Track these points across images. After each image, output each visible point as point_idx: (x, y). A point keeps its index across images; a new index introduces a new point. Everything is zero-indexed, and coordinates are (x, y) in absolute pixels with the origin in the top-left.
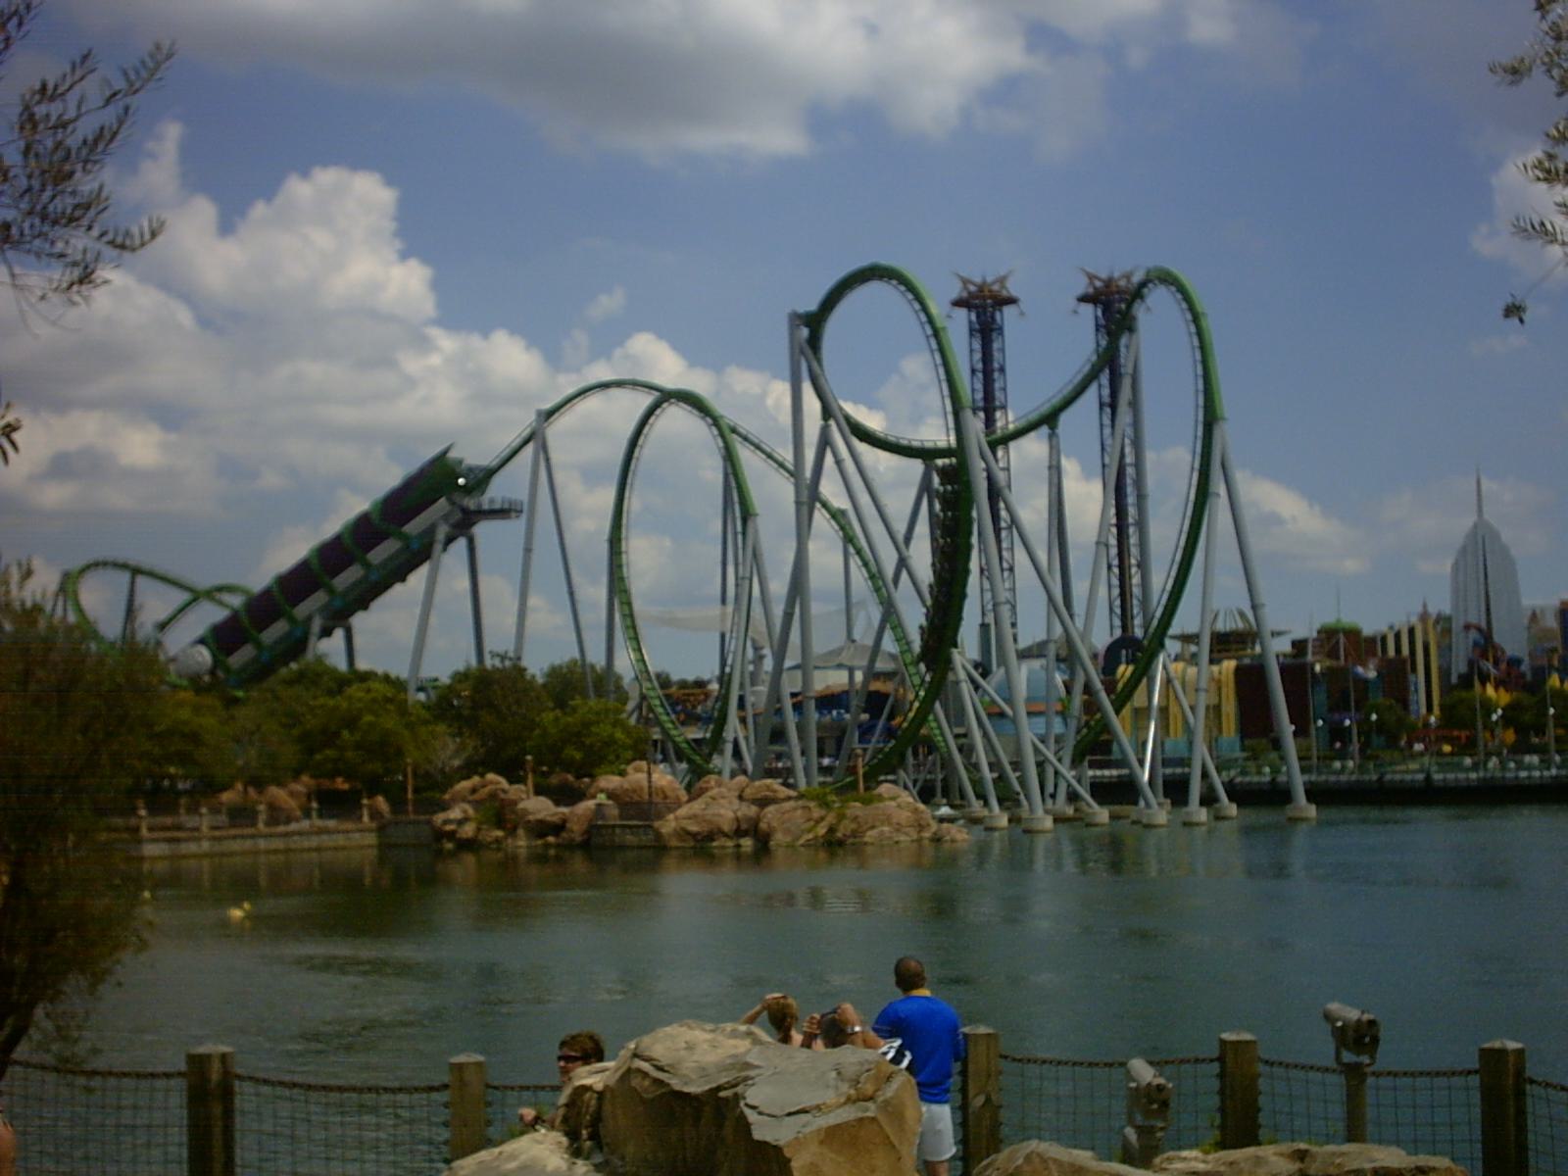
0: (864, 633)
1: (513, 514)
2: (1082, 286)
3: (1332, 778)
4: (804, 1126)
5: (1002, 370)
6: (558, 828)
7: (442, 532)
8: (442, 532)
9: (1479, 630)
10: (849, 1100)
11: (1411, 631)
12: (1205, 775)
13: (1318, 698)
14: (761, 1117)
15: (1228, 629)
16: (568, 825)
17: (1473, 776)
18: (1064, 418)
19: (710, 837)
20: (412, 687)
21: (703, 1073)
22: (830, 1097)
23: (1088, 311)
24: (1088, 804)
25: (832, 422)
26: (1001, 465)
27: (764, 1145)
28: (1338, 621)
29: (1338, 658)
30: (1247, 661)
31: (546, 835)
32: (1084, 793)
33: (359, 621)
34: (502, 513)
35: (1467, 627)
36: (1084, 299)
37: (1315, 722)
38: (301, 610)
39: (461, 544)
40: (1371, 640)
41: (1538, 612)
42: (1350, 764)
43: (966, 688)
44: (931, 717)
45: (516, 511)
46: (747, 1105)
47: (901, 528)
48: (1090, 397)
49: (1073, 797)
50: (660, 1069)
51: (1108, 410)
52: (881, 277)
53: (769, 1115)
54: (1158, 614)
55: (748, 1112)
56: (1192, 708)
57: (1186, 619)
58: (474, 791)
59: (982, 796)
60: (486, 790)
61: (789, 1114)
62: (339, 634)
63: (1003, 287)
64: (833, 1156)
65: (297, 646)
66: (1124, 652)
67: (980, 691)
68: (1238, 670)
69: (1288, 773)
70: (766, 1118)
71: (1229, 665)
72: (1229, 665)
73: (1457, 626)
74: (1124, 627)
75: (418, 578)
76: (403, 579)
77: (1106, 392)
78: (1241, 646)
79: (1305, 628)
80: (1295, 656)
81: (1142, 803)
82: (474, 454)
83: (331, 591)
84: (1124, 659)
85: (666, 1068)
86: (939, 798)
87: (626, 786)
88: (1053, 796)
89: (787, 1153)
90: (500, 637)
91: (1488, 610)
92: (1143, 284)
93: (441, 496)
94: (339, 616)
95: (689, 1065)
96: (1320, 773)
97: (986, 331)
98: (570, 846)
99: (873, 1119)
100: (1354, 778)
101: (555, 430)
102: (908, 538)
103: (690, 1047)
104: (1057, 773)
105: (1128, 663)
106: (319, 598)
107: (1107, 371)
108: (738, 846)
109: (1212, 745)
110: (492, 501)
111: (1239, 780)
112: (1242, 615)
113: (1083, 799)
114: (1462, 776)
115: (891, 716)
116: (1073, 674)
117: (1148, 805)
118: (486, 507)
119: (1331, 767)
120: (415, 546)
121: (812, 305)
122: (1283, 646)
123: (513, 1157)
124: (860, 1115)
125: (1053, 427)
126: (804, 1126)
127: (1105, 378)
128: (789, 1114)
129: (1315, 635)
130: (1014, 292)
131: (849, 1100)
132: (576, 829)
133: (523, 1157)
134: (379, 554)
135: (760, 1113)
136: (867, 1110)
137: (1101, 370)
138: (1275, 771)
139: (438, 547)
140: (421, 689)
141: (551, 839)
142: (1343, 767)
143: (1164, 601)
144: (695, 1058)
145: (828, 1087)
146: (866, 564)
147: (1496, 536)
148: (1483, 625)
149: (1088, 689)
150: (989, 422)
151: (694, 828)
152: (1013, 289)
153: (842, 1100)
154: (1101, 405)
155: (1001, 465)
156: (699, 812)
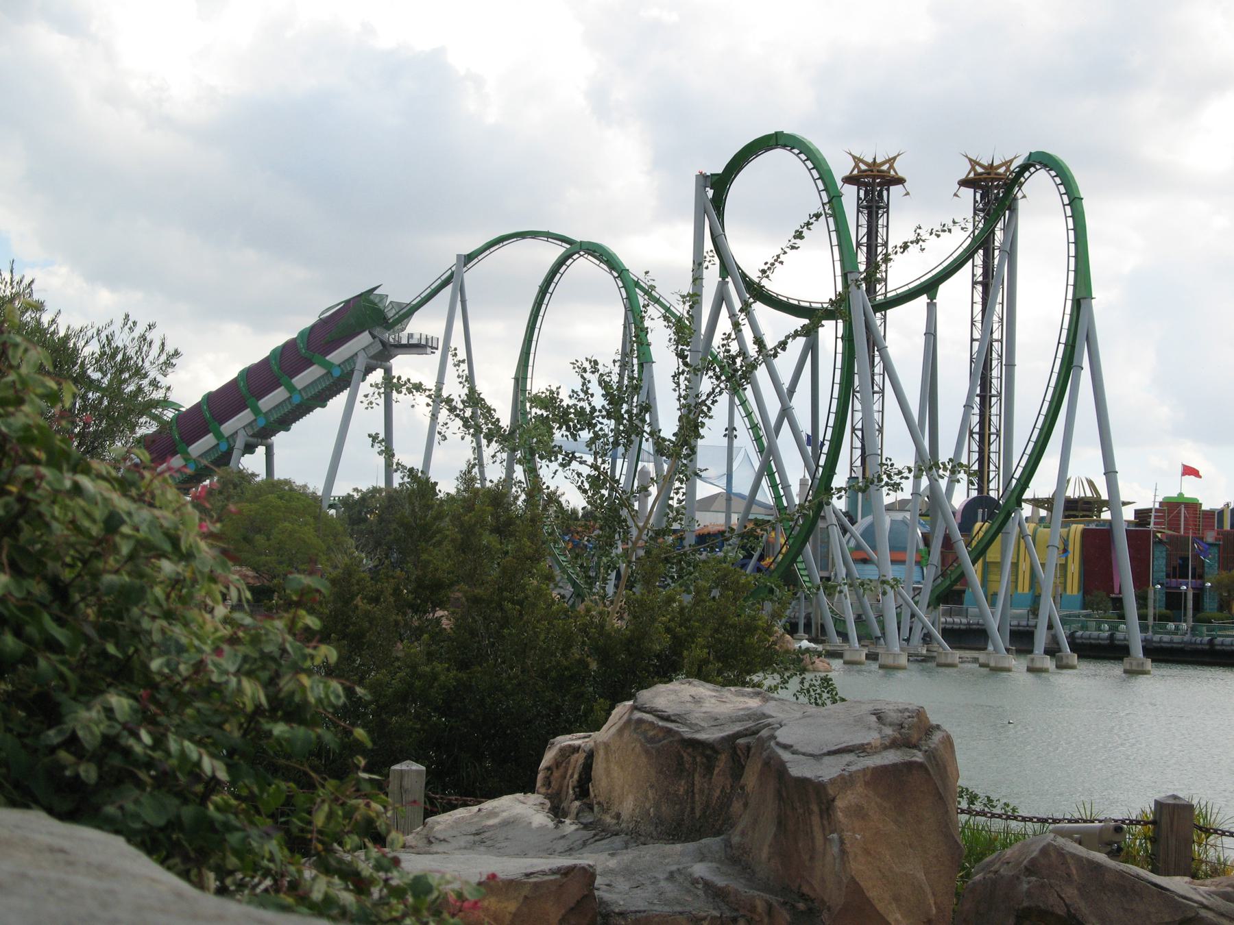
0: (742, 485)
1: (429, 350)
2: (964, 170)
3: (1166, 638)
4: (848, 765)
8: (360, 364)
10: (894, 744)
12: (1050, 627)
13: (1158, 563)
14: (795, 756)
15: (1076, 497)
18: (943, 289)
20: (325, 505)
21: (716, 721)
22: (872, 737)
23: (968, 193)
24: (940, 645)
25: (729, 279)
27: (803, 782)
28: (1181, 494)
29: (1177, 529)
30: (1093, 526)
32: (937, 634)
33: (279, 439)
36: (965, 183)
37: (1153, 586)
38: (228, 428)
40: (1210, 513)
42: (1184, 626)
43: (835, 532)
44: (800, 558)
45: (432, 348)
46: (778, 744)
47: (786, 381)
48: (963, 277)
49: (927, 638)
50: (667, 719)
51: (979, 288)
52: (784, 146)
53: (804, 754)
54: (1017, 475)
55: (780, 752)
56: (1043, 565)
57: (1042, 485)
59: (844, 636)
61: (830, 753)
62: (261, 450)
63: (891, 167)
64: (878, 800)
65: (224, 458)
66: (980, 511)
67: (848, 535)
68: (1085, 533)
69: (1128, 631)
70: (801, 757)
71: (1077, 528)
72: (1077, 528)
74: (980, 490)
75: (338, 402)
76: (323, 404)
77: (979, 271)
78: (1088, 513)
79: (1147, 501)
80: (1137, 525)
81: (991, 648)
82: (397, 292)
83: (256, 411)
84: (980, 517)
85: (673, 718)
86: (801, 633)
88: (908, 640)
89: (831, 791)
90: (409, 455)
92: (1024, 168)
93: (364, 331)
94: (262, 435)
95: (697, 715)
96: (1155, 633)
97: (874, 207)
99: (921, 765)
100: (1187, 638)
101: (472, 276)
102: (792, 390)
103: (697, 700)
104: (913, 616)
105: (984, 521)
106: (245, 416)
107: (981, 252)
109: (1059, 598)
110: (410, 336)
111: (1079, 633)
112: (1091, 484)
113: (937, 640)
115: (761, 558)
116: (933, 525)
117: (996, 650)
118: (404, 341)
119: (1165, 628)
120: (337, 373)
121: (719, 169)
122: (1128, 514)
123: (492, 814)
124: (907, 758)
125: (932, 297)
126: (848, 765)
127: (979, 258)
128: (830, 753)
129: (1157, 506)
130: (901, 174)
131: (894, 744)
133: (505, 814)
134: (303, 379)
135: (794, 753)
136: (915, 755)
137: (976, 251)
138: (1114, 628)
139: (357, 375)
140: (331, 506)
142: (1177, 628)
143: (1023, 463)
144: (704, 710)
145: (870, 728)
146: (749, 415)
149: (948, 543)
150: (871, 291)
152: (900, 169)
153: (887, 742)
154: (974, 283)
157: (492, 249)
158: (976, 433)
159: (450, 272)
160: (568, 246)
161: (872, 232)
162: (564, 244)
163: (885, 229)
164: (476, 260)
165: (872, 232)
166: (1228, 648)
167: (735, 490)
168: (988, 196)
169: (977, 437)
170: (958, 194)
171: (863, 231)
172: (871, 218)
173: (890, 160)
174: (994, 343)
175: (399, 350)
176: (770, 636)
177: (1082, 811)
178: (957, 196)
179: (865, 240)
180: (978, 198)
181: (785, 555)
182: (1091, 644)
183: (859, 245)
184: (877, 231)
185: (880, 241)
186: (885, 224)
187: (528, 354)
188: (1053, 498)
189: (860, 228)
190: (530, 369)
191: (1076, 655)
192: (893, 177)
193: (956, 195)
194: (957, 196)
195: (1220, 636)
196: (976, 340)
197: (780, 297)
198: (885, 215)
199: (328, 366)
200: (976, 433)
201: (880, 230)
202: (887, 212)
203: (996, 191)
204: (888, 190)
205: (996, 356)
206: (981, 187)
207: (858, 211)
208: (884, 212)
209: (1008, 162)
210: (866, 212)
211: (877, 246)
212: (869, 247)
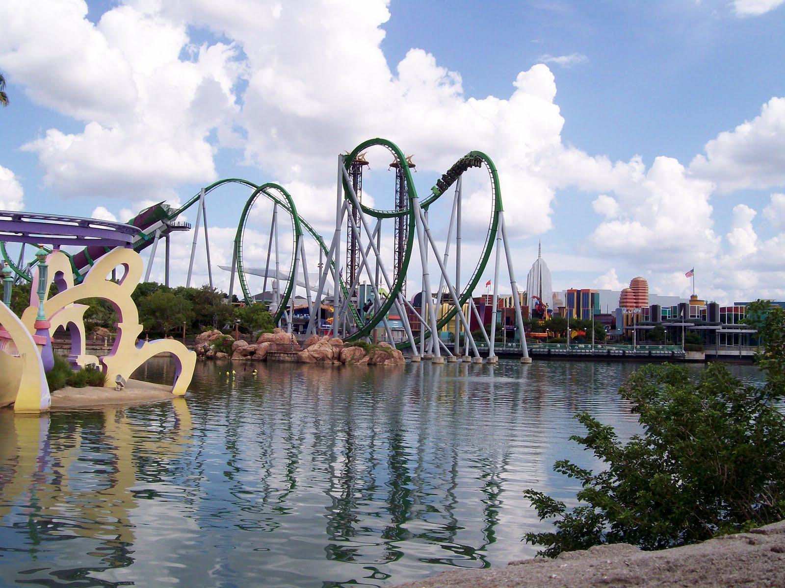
5: (397, 191)
6: (252, 353)
7: (157, 235)
8: (157, 235)
9: (538, 299)
11: (510, 299)
16: (257, 352)
17: (516, 349)
19: (323, 359)
26: (357, 225)
31: (247, 356)
34: (184, 228)
35: (534, 297)
36: (392, 165)
39: (164, 238)
41: (556, 293)
58: (209, 336)
60: (215, 336)
63: (363, 157)
73: (529, 296)
87: (277, 337)
91: (541, 292)
98: (258, 360)
108: (333, 363)
114: (658, 352)
120: (147, 238)
130: (367, 160)
132: (261, 354)
141: (249, 357)
142: (512, 345)
147: (545, 264)
148: (539, 297)
151: (316, 355)
155: (357, 225)
156: (317, 349)
157: (216, 186)
159: (197, 195)
160: (256, 189)
162: (253, 187)
164: (209, 191)
166: (542, 353)
169: (350, 267)
175: (173, 229)
176: (92, 347)
177: (637, 418)
179: (399, 190)
180: (398, 171)
182: (536, 354)
184: (357, 183)
188: (437, 294)
191: (531, 359)
192: (364, 162)
195: (534, 348)
199: (143, 236)
202: (361, 176)
204: (362, 167)
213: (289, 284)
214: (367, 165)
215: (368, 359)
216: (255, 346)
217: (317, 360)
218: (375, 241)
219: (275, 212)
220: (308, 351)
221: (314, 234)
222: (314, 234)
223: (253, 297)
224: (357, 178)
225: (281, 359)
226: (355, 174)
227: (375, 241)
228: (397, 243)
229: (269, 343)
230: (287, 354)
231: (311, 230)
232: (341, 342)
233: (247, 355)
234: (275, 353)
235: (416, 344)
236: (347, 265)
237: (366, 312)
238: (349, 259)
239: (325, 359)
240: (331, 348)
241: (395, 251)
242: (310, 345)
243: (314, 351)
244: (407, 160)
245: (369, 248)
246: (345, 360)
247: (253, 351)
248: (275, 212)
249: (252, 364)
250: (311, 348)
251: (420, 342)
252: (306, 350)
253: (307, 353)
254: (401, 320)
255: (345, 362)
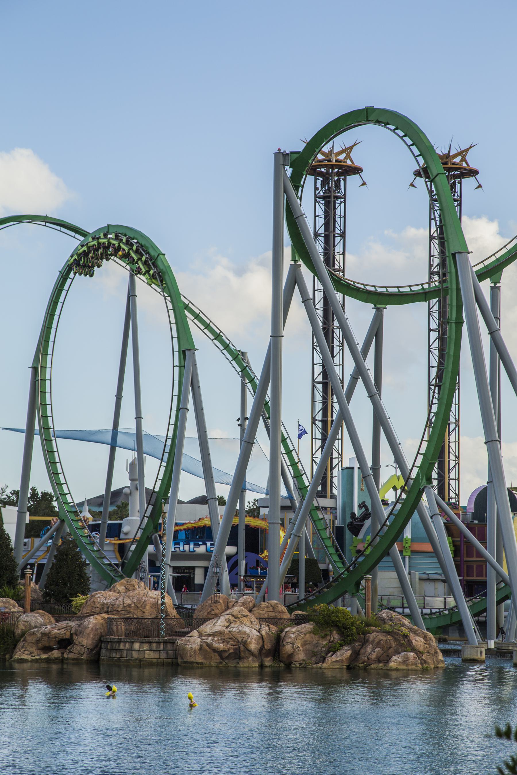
5: (343, 235)
63: (348, 157)
98: (77, 662)
151: (221, 646)
158: (319, 420)
161: (330, 223)
162: (77, 236)
163: (342, 219)
165: (330, 223)
167: (160, 461)
168: (329, 184)
169: (319, 424)
170: (414, 183)
171: (321, 221)
172: (329, 208)
173: (462, 152)
174: (335, 330)
178: (413, 186)
180: (319, 185)
181: (390, 527)
183: (316, 235)
184: (335, 221)
185: (337, 231)
186: (342, 214)
187: (50, 328)
189: (317, 218)
190: (51, 344)
192: (350, 167)
193: (412, 185)
194: (413, 186)
196: (434, 330)
197: (357, 285)
198: (343, 205)
200: (319, 420)
201: (338, 220)
202: (460, 203)
203: (336, 178)
204: (345, 180)
205: (338, 343)
206: (321, 174)
207: (316, 201)
208: (341, 202)
209: (348, 148)
210: (323, 202)
211: (334, 237)
212: (327, 238)
213: (163, 469)
214: (357, 175)
215: (349, 653)
216: (72, 624)
217: (222, 658)
218: (369, 363)
219: (131, 296)
220: (201, 635)
221: (226, 347)
222: (226, 347)
223: (81, 504)
224: (335, 209)
225: (135, 655)
226: (329, 197)
227: (369, 363)
228: (434, 363)
229: (106, 616)
230: (150, 643)
231: (218, 337)
232: (283, 612)
233: (51, 649)
234: (119, 641)
235: (474, 615)
236: (314, 420)
237: (357, 535)
238: (318, 406)
239: (242, 654)
240: (258, 627)
241: (313, 381)
242: (205, 620)
243: (214, 635)
244: (457, 160)
245: (354, 379)
246: (291, 656)
247: (68, 636)
248: (131, 296)
249: (62, 669)
250: (208, 628)
251: (485, 610)
252: (195, 633)
253: (199, 640)
254: (436, 552)
255: (291, 663)
